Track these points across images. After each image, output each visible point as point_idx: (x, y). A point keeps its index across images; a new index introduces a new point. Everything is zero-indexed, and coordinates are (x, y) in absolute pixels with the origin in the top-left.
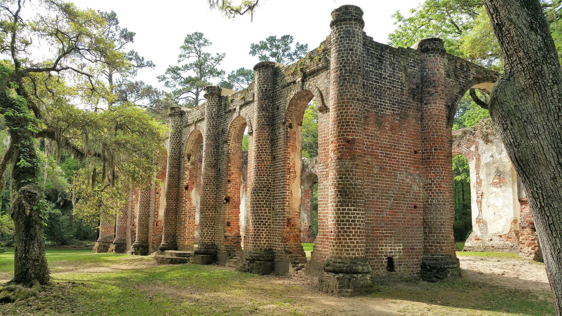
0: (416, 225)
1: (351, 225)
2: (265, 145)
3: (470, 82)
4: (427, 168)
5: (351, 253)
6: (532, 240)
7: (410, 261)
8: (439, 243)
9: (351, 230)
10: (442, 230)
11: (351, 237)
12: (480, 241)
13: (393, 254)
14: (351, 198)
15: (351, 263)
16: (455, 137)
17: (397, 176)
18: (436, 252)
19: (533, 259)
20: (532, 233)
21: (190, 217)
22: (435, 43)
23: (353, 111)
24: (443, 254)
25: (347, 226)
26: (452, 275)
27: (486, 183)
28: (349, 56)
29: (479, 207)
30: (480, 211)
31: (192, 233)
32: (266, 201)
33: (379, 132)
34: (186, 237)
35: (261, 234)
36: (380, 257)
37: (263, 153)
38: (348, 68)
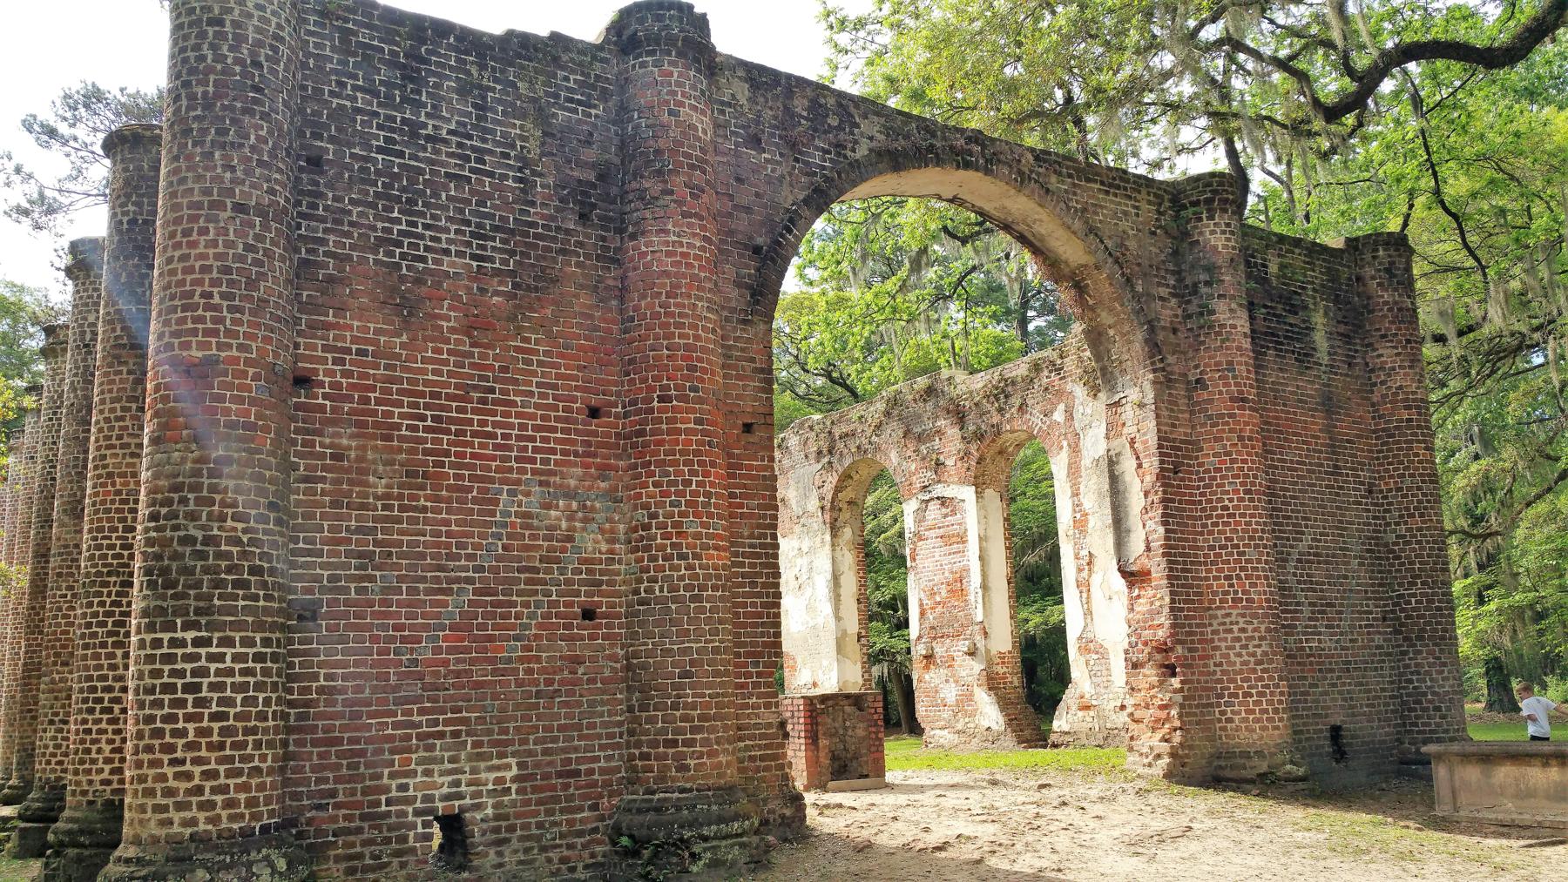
0: (592, 681)
1: (181, 703)
2: (122, 419)
3: (854, 165)
4: (635, 466)
5: (176, 820)
6: (1162, 707)
7: (554, 824)
8: (674, 743)
9: (180, 725)
10: (687, 696)
11: (179, 754)
12: (1092, 713)
13: (468, 801)
14: (185, 596)
15: (167, 860)
16: (1013, 383)
17: (496, 502)
18: (662, 778)
19: (1165, 776)
20: (1161, 683)
22: (659, 18)
23: (211, 251)
24: (688, 785)
25: (166, 710)
26: (715, 864)
27: (1099, 524)
28: (205, 47)
29: (1084, 601)
30: (1088, 613)
32: (115, 624)
33: (404, 338)
35: (94, 748)
36: (393, 819)
37: (113, 447)
38: (200, 90)
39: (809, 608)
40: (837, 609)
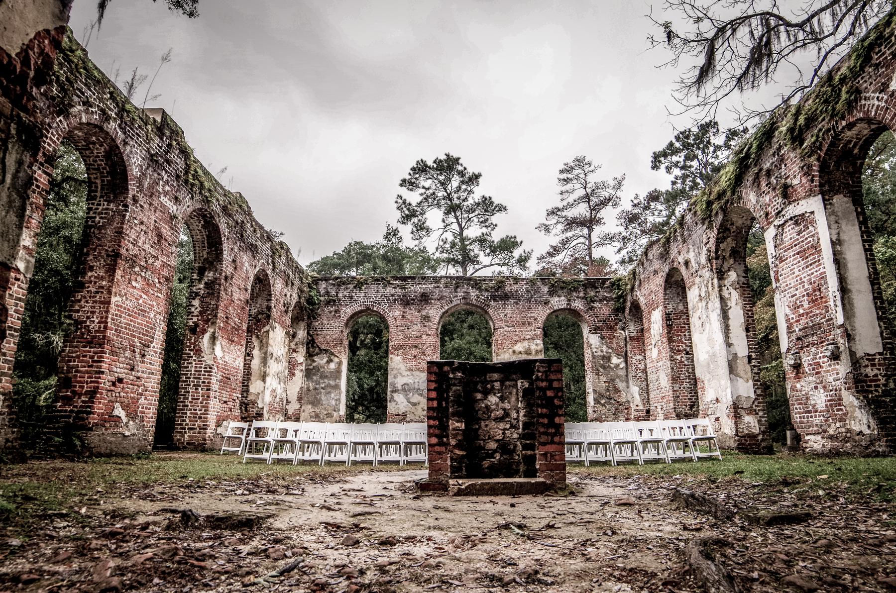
21: (196, 387)
31: (200, 418)
34: (187, 424)
39: (710, 340)
40: (727, 336)
